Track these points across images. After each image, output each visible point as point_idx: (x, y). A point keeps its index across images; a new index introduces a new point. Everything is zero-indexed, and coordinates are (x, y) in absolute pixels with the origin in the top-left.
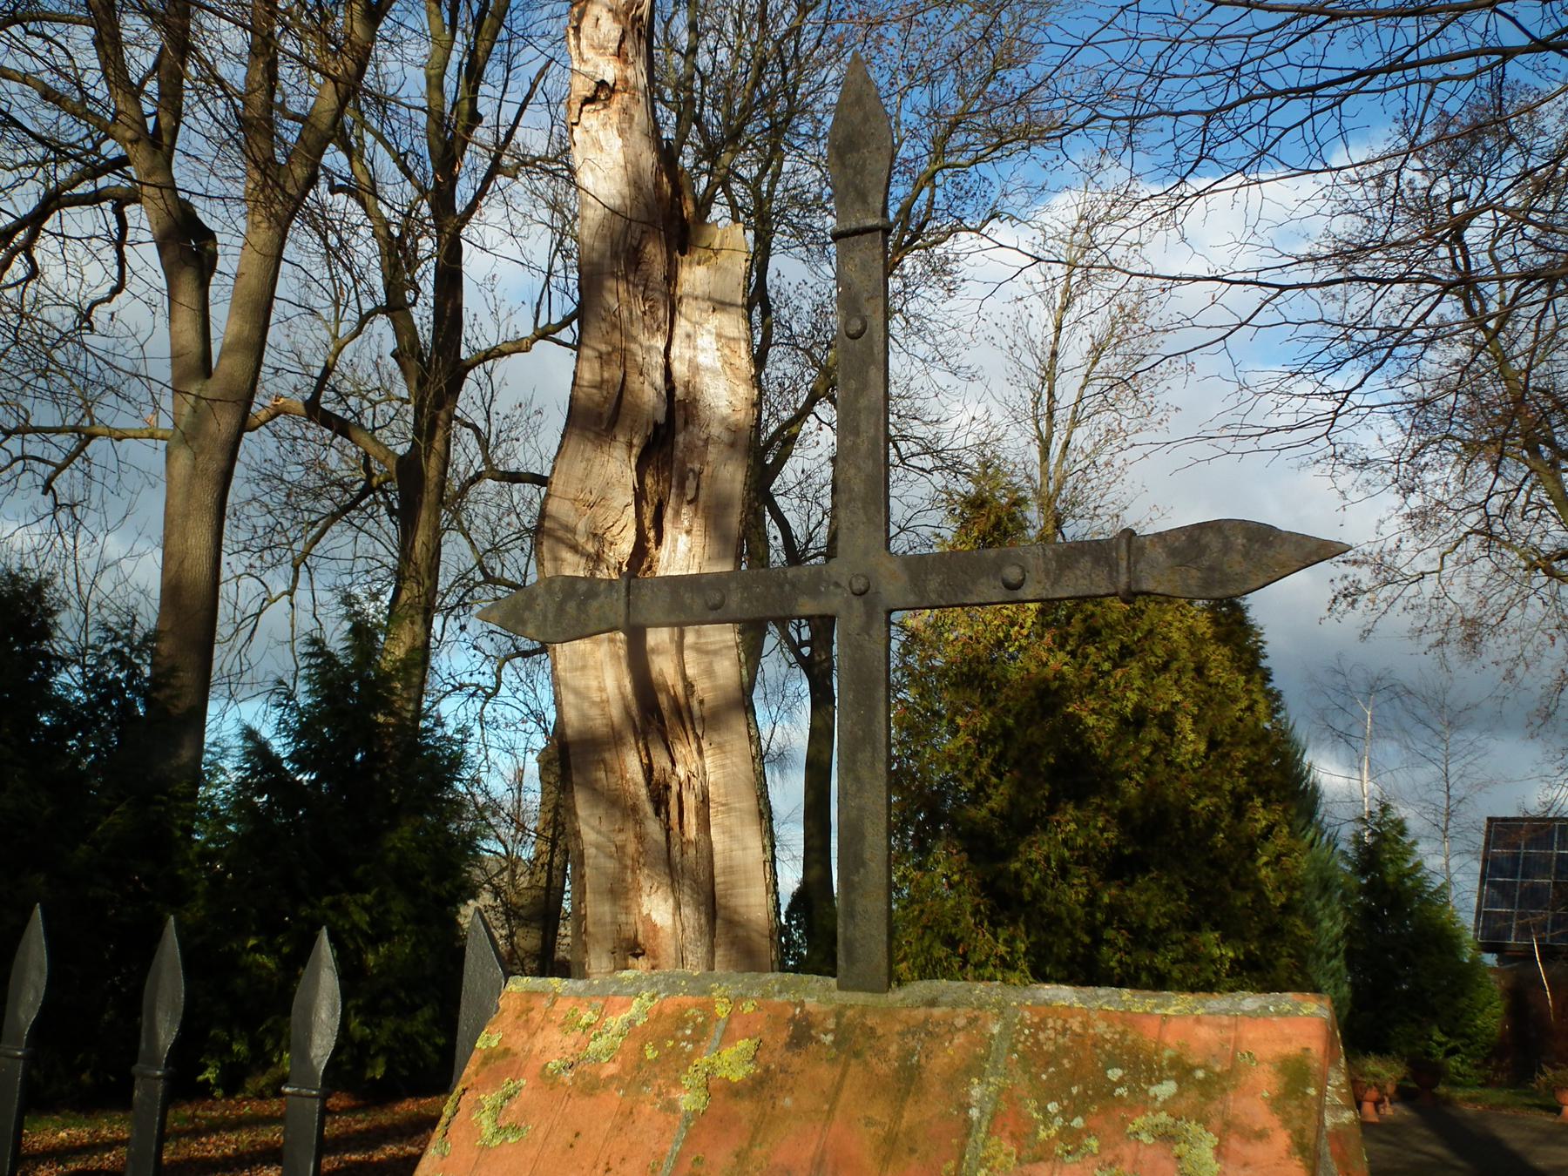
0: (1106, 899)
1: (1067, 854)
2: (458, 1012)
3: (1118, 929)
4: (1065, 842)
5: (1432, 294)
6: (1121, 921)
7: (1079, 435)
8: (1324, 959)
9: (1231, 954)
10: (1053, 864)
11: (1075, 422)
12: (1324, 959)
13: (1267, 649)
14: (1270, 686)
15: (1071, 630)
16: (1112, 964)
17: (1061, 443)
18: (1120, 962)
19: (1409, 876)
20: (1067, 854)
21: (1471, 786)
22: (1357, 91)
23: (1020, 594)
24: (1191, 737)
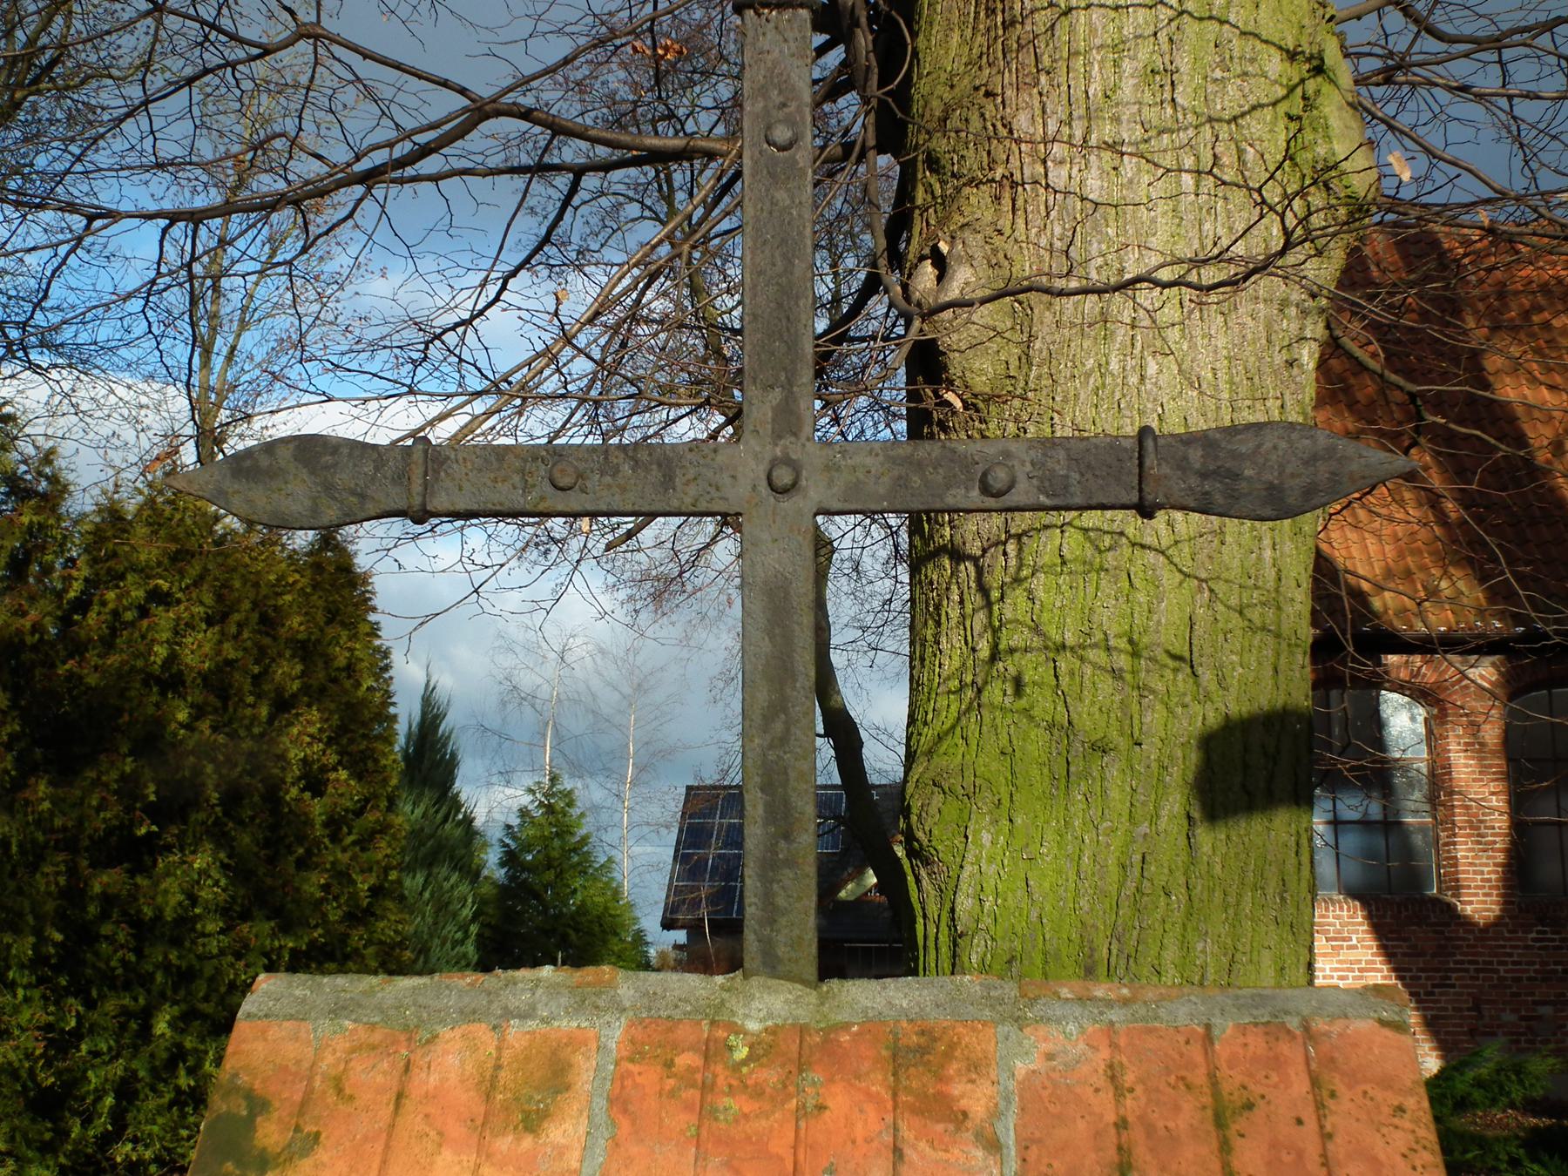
0: (97, 889)
1: (41, 837)
2: (820, 930)
3: (118, 923)
4: (38, 823)
5: (68, 242)
6: (125, 913)
7: (248, 341)
8: (448, 945)
9: (291, 945)
10: (14, 849)
11: (244, 325)
12: (448, 945)
13: (376, 602)
14: (377, 642)
15: (75, 573)
16: (113, 964)
17: (225, 351)
18: (123, 962)
19: (575, 850)
20: (41, 837)
21: (654, 754)
22: (1466, 55)
23: (1008, 500)
24: (250, 699)
